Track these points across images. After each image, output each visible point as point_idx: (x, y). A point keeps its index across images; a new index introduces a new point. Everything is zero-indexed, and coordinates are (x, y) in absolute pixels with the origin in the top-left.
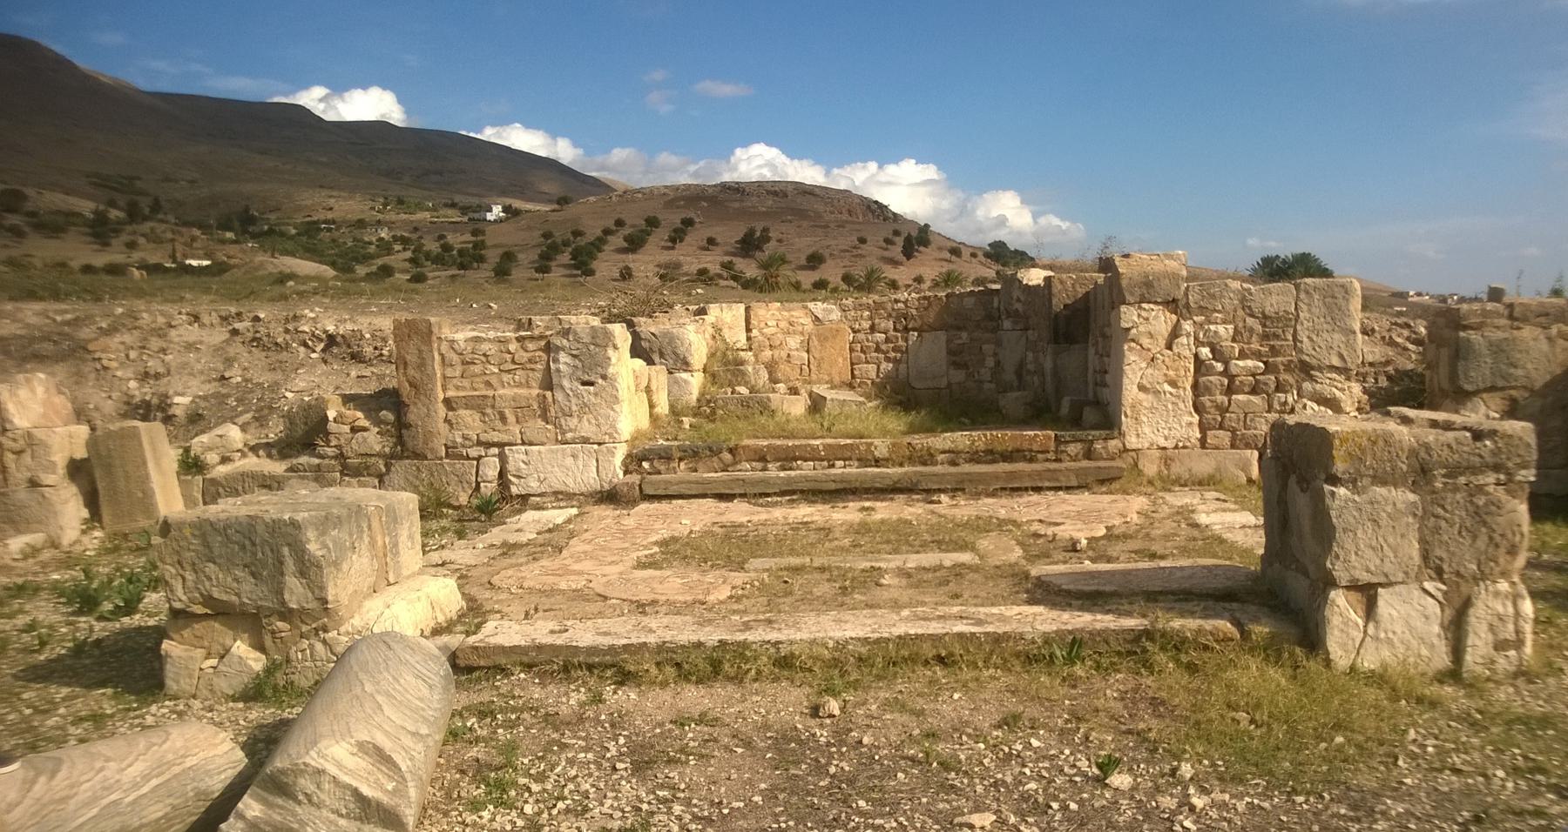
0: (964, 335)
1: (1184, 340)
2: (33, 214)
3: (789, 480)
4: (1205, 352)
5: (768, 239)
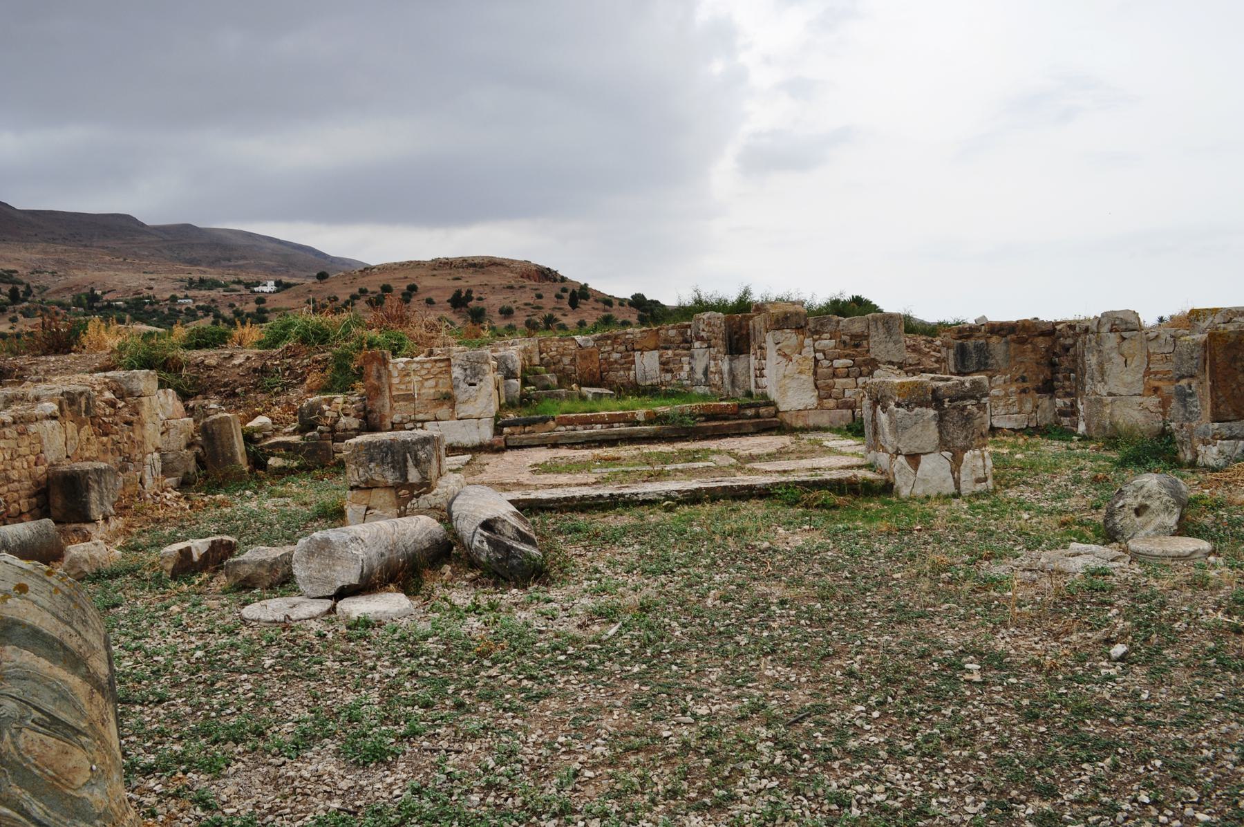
0: (670, 352)
3: (590, 435)
4: (820, 356)
5: (472, 299)
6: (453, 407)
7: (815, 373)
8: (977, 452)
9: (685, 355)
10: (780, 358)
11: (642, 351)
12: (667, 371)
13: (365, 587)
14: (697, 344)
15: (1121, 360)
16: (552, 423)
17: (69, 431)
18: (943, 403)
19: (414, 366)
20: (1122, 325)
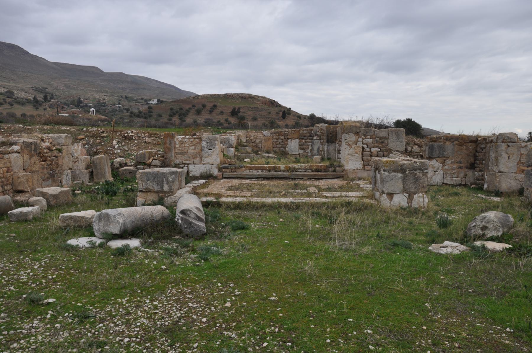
0: (304, 140)
1: (359, 143)
2: (15, 99)
4: (365, 146)
5: (240, 112)
6: (201, 158)
7: (362, 154)
8: (421, 195)
9: (310, 142)
10: (347, 146)
11: (291, 139)
12: (302, 149)
13: (124, 235)
14: (315, 138)
15: (507, 156)
16: (243, 168)
17: (25, 158)
18: (405, 172)
19: (186, 140)
20: (508, 140)
